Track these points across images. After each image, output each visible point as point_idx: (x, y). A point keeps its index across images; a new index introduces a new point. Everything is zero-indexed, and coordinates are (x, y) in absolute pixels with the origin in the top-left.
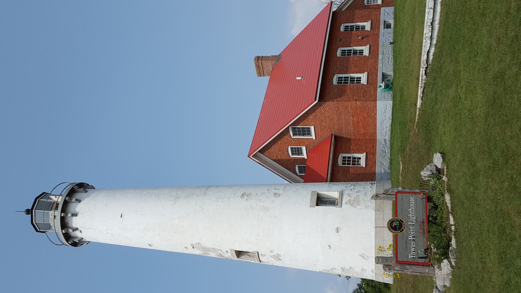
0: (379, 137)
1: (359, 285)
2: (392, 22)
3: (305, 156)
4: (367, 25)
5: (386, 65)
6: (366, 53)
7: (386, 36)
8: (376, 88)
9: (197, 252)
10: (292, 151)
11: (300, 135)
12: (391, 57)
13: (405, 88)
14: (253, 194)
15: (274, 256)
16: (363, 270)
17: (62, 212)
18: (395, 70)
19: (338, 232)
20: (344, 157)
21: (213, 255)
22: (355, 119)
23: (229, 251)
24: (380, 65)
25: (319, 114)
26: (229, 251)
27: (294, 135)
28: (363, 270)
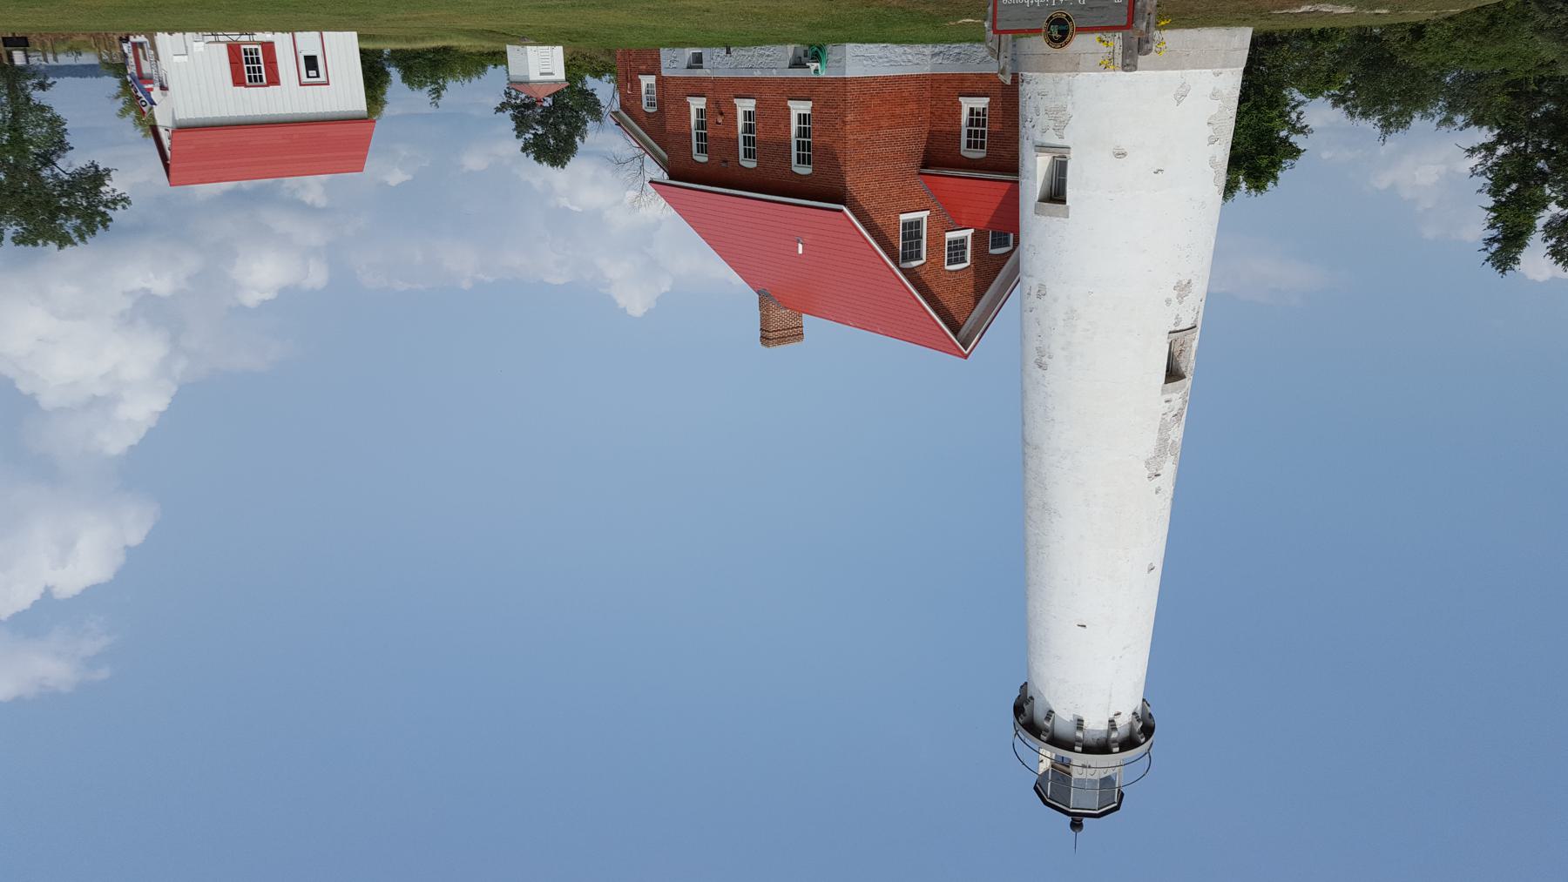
0: (926, 70)
1: (1335, 105)
2: (689, 52)
3: (969, 233)
4: (696, 104)
5: (773, 61)
6: (804, 107)
7: (718, 65)
8: (820, 80)
9: (1169, 468)
10: (957, 262)
11: (919, 245)
12: (758, 50)
13: (807, 19)
14: (1037, 344)
15: (1181, 298)
16: (1215, 95)
17: (1072, 750)
18: (786, 41)
19: (1124, 154)
20: (969, 146)
21: (1177, 433)
22: (884, 123)
23: (1167, 397)
24: (774, 74)
25: (874, 204)
26: (1167, 397)
27: (919, 257)
28: (1215, 95)
